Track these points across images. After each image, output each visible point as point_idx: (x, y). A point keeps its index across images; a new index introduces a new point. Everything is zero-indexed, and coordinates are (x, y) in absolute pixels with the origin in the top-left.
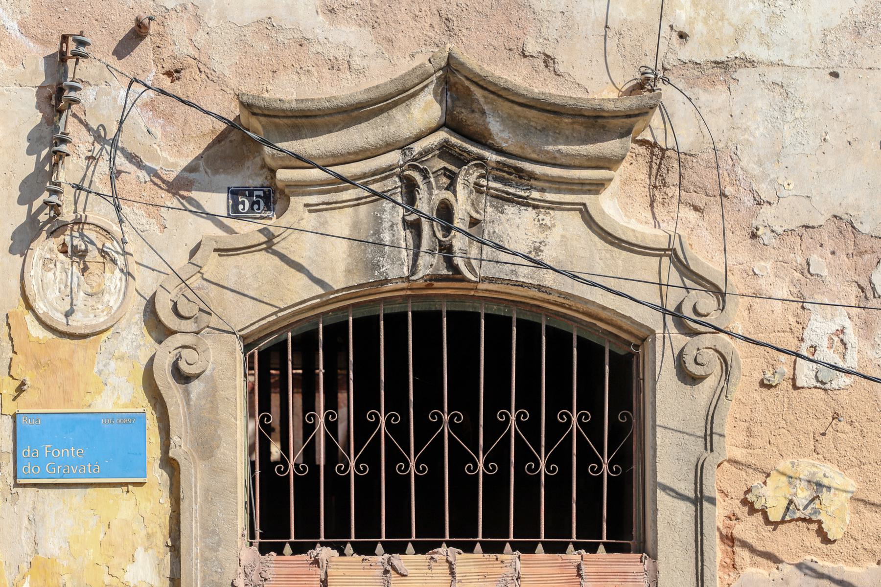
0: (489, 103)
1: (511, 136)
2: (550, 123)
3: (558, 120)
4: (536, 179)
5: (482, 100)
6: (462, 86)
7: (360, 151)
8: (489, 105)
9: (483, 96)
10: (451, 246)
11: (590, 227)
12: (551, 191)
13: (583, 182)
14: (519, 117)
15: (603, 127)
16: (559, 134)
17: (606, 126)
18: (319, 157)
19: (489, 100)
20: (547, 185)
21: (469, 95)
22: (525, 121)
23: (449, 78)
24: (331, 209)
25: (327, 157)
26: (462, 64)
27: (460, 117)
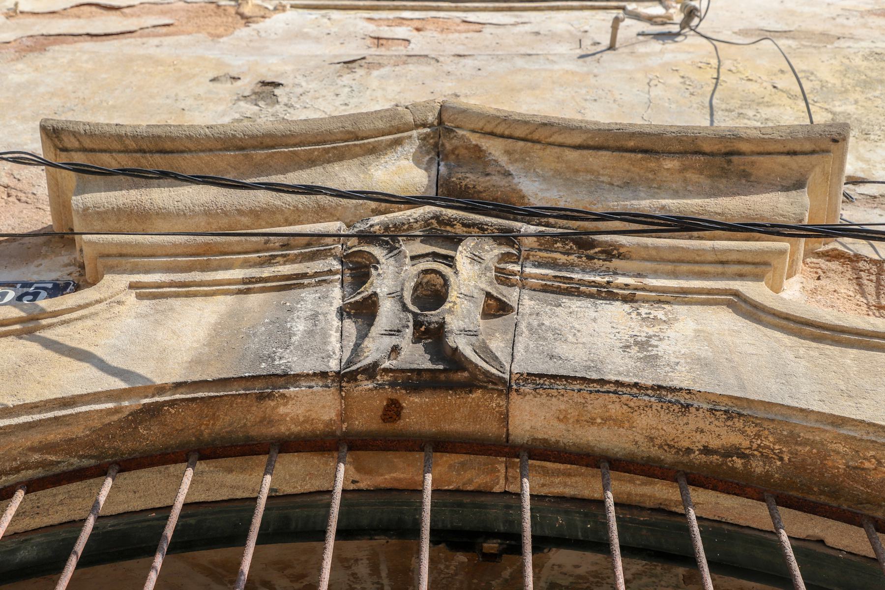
0: (516, 161)
1: (562, 194)
3: (652, 165)
5: (503, 160)
6: (467, 148)
8: (516, 165)
10: (442, 325)
11: (759, 321)
12: (656, 274)
13: (724, 258)
14: (577, 171)
15: (745, 175)
16: (659, 188)
17: (750, 175)
19: (517, 156)
23: (443, 145)
24: (187, 295)
25: (194, 214)
26: (464, 112)
27: (464, 183)
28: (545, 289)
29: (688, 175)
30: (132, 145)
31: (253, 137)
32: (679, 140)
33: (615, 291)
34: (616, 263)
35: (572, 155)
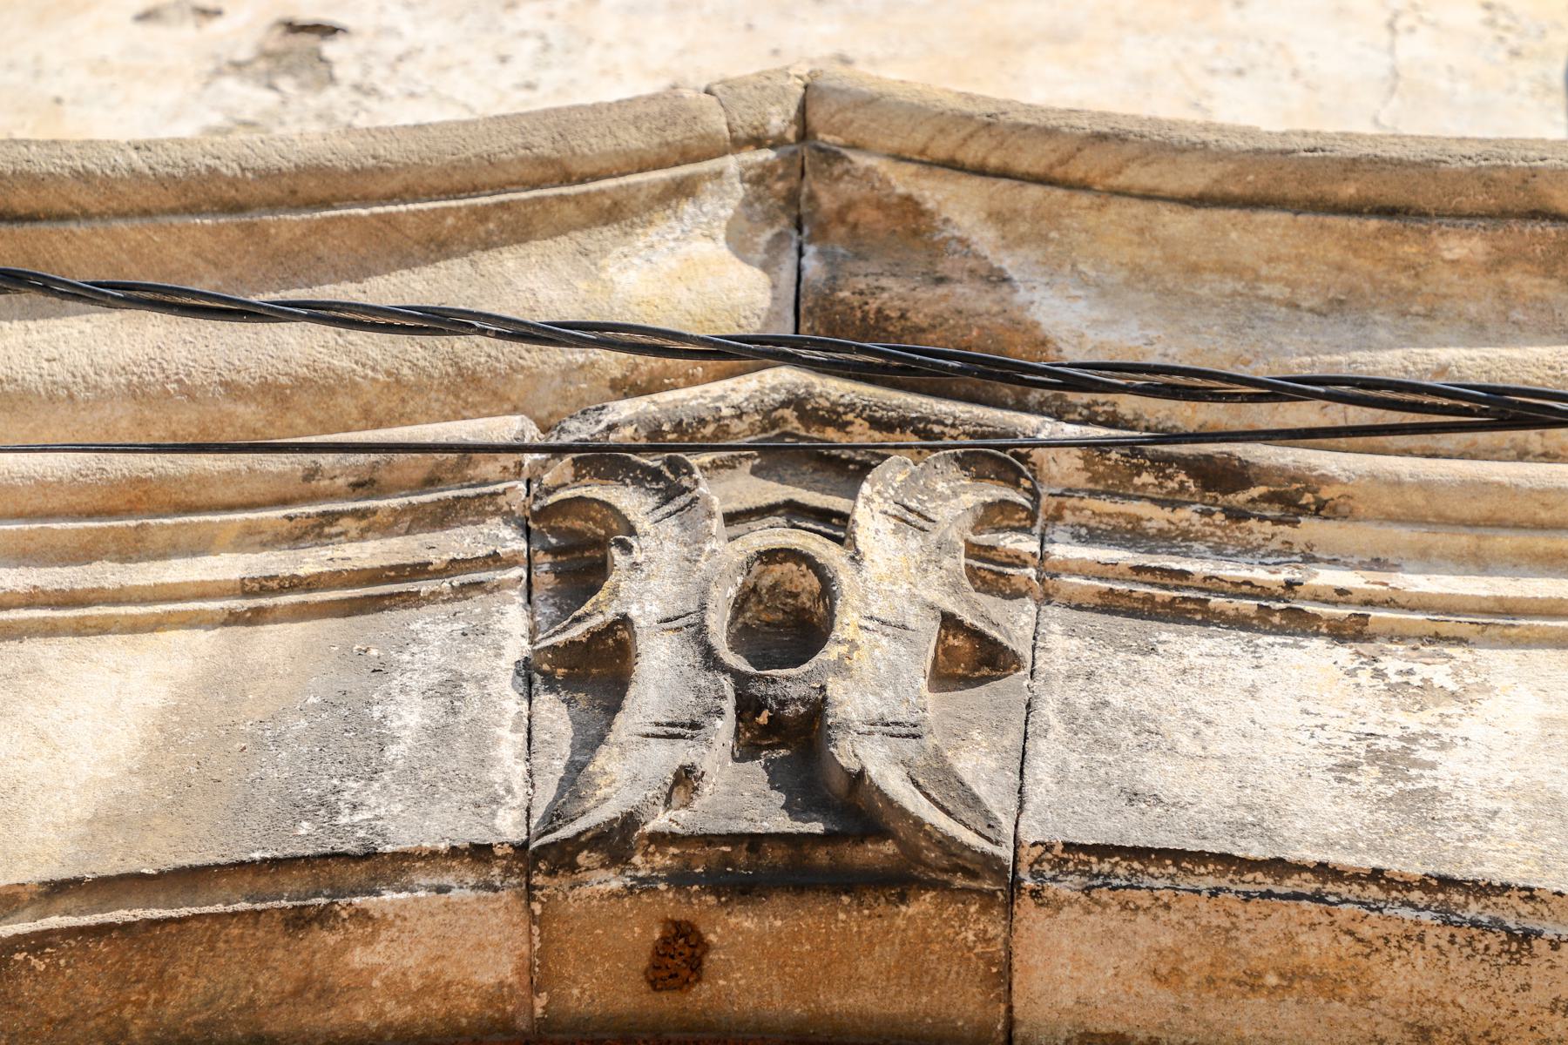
0: (1021, 240)
1: (1152, 333)
2: (1371, 277)
3: (1410, 250)
4: (1321, 510)
5: (985, 239)
6: (880, 205)
7: (302, 384)
8: (1023, 251)
9: (990, 215)
12: (1426, 560)
14: (1194, 269)
16: (1429, 315)
18: (52, 398)
19: (1024, 228)
20: (1404, 534)
21: (916, 233)
22: (1230, 285)
23: (812, 197)
24: (80, 629)
25: (102, 396)
27: (874, 305)
28: (1109, 605)
29: (1513, 278)
31: (266, 175)
32: (1486, 179)
35: (1182, 224)
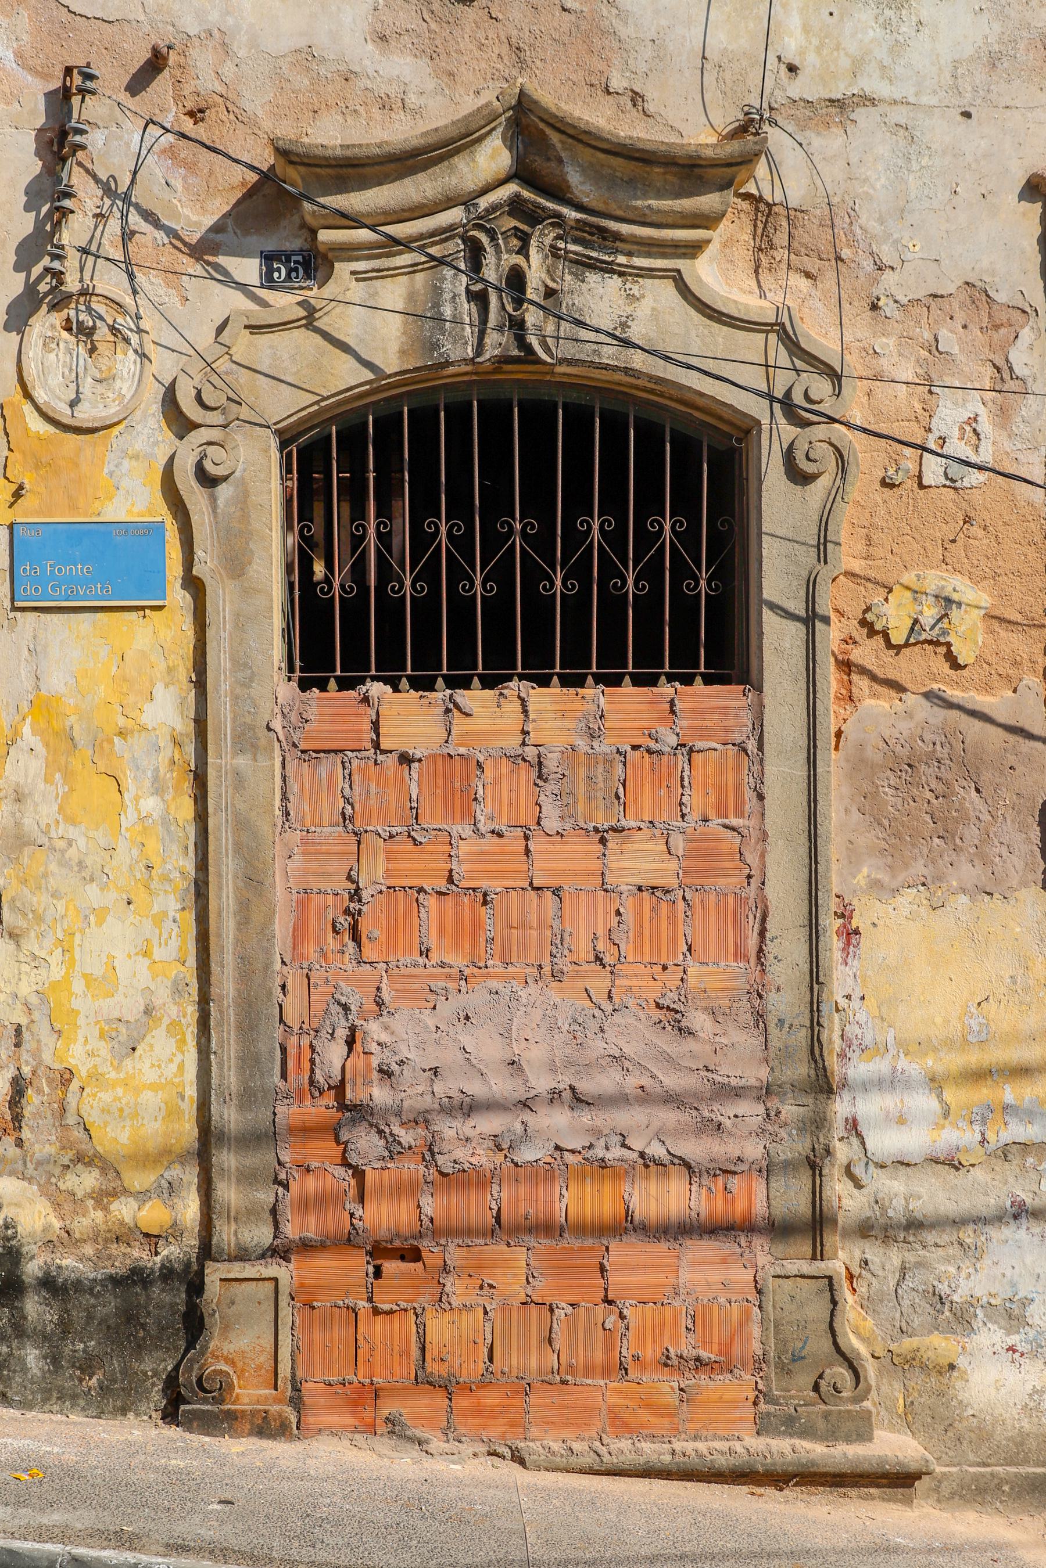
3: (648, 169)
11: (685, 298)
14: (603, 165)
15: (700, 177)
24: (382, 277)
28: (577, 262)
29: (667, 176)
30: (334, 163)
31: (406, 152)
32: (665, 156)
33: (613, 225)
34: (618, 244)
35: (601, 156)
